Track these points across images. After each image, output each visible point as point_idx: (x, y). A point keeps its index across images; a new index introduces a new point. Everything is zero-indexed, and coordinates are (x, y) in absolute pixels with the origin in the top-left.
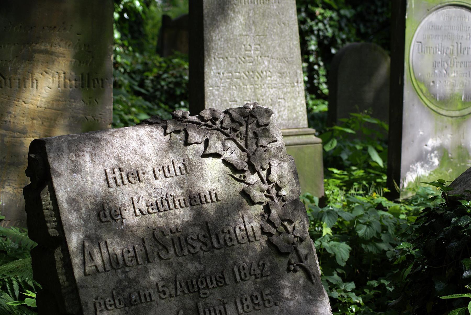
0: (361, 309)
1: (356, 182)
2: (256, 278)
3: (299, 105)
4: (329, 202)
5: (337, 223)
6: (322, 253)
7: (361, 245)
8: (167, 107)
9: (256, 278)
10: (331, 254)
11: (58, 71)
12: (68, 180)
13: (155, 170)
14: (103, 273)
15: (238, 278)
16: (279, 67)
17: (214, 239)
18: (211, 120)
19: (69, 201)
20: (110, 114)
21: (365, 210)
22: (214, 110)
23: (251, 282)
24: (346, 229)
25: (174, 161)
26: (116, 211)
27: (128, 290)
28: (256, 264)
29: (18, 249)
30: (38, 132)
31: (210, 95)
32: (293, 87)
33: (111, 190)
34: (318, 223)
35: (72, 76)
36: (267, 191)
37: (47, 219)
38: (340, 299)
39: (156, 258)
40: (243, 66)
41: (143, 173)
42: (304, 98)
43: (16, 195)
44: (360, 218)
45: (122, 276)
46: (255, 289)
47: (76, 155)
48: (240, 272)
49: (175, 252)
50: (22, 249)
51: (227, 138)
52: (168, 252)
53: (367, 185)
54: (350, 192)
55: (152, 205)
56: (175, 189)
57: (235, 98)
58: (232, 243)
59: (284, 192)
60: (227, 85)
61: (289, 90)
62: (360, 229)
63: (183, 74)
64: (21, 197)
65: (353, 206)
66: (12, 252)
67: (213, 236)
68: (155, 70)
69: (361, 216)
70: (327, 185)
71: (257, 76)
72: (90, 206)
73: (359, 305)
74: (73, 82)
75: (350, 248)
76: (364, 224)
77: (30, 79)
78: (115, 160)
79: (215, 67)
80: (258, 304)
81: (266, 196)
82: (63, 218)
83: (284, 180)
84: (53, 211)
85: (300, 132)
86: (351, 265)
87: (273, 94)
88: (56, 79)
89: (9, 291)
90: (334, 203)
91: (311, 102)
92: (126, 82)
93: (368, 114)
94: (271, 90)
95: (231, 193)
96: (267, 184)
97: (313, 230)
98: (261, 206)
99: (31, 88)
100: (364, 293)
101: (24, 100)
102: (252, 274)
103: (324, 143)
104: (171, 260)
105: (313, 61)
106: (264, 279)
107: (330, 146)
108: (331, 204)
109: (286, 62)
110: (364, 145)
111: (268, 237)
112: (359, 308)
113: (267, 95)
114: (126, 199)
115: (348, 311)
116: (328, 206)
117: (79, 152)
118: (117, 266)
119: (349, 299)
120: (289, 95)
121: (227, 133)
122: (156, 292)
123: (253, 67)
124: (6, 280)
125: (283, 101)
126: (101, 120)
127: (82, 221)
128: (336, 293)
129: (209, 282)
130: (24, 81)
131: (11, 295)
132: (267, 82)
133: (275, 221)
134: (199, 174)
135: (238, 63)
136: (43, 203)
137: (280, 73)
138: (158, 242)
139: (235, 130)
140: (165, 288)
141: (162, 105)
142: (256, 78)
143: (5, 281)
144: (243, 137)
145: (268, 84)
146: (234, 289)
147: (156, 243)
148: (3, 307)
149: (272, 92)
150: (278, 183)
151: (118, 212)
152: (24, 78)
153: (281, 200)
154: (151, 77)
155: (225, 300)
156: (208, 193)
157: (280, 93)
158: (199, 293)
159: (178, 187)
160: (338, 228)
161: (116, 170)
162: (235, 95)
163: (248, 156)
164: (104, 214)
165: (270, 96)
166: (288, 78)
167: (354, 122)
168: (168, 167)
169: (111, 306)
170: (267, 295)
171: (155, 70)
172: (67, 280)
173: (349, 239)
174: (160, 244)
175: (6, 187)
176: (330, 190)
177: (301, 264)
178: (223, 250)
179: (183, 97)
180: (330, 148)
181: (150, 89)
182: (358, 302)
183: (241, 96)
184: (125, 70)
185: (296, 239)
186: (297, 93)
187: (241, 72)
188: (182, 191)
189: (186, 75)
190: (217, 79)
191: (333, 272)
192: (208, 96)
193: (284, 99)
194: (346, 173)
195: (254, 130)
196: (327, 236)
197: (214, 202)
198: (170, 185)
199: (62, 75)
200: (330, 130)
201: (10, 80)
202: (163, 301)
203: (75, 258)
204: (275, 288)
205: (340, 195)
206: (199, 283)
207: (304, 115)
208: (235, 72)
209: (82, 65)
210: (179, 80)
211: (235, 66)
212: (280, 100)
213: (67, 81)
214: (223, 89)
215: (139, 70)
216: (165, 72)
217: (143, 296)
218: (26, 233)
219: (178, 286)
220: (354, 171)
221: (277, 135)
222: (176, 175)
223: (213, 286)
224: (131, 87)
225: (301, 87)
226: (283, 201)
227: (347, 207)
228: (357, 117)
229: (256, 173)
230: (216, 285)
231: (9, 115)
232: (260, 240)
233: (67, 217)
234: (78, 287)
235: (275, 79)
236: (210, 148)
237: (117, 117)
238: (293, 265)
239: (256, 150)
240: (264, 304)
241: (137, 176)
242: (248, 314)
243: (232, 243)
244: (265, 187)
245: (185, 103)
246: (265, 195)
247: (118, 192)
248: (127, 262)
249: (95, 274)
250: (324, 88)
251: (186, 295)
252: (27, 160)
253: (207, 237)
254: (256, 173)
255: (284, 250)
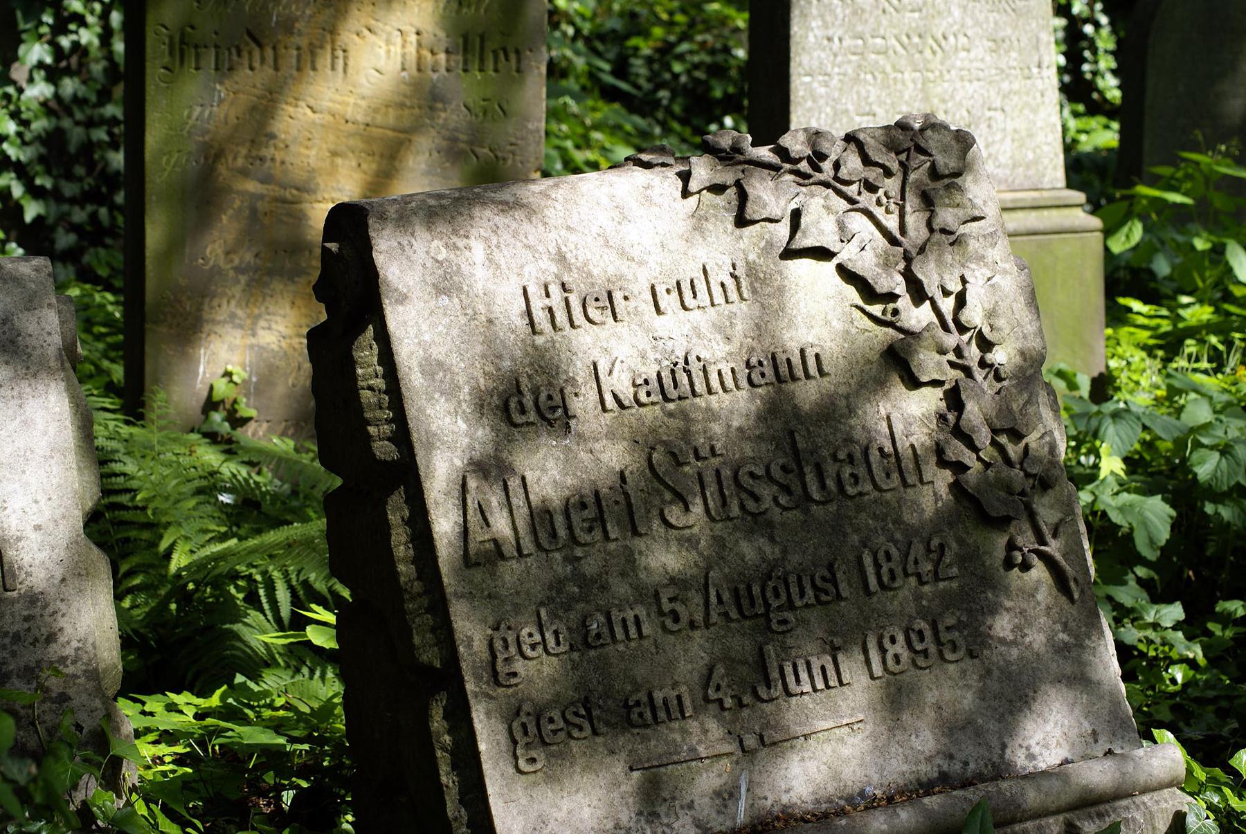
0: (1198, 676)
1: (1192, 337)
2: (921, 583)
3: (1042, 128)
4: (1118, 389)
5: (1137, 446)
6: (1097, 523)
7: (1203, 506)
8: (687, 132)
9: (921, 583)
10: (1120, 527)
11: (402, 28)
12: (426, 314)
13: (657, 289)
14: (514, 562)
15: (872, 581)
16: (992, 25)
17: (810, 478)
18: (809, 159)
19: (427, 369)
20: (538, 143)
21: (1215, 412)
22: (817, 133)
23: (907, 593)
24: (1162, 461)
25: (708, 268)
26: (550, 397)
27: (580, 606)
28: (921, 546)
29: (289, 497)
30: (347, 188)
31: (803, 97)
32: (1029, 78)
33: (539, 340)
34: (1088, 445)
35: (439, 40)
36: (954, 350)
37: (368, 415)
38: (1142, 647)
39: (656, 523)
40: (895, 21)
41: (626, 298)
42: (1058, 107)
43: (285, 353)
44: (1203, 432)
45: (563, 570)
46: (918, 613)
47: (447, 246)
48: (878, 566)
49: (707, 510)
50: (301, 496)
51: (850, 207)
52: (687, 509)
53: (1221, 347)
54: (1174, 365)
55: (646, 382)
56: (710, 341)
57: (870, 105)
58: (859, 488)
59: (999, 356)
60: (850, 71)
61: (1016, 86)
62: (1202, 462)
63: (731, 43)
64: (300, 359)
65: (1182, 402)
66: (273, 503)
67: (807, 469)
68: (658, 32)
69: (1206, 427)
70: (1112, 342)
71: (931, 48)
72: (482, 381)
73: (1192, 664)
74: (442, 57)
75: (1174, 513)
76: (1212, 448)
77: (329, 47)
78: (552, 260)
79: (820, 23)
80: (925, 653)
81: (952, 365)
82: (411, 412)
83: (1001, 322)
84: (385, 393)
85: (1044, 199)
86: (1175, 559)
87: (972, 97)
88: (397, 49)
89: (266, 606)
90: (1131, 392)
91: (1073, 124)
92: (580, 63)
93: (1227, 154)
94: (967, 84)
95: (859, 356)
96: (956, 333)
97: (1074, 463)
98: (939, 392)
99: (329, 72)
100: (1210, 634)
101: (312, 102)
102: (910, 571)
103: (1108, 232)
104: (696, 530)
105: (1081, 12)
106: (941, 585)
107: (1123, 238)
108: (1123, 395)
109: (1009, 10)
110: (1214, 239)
111: (954, 474)
112: (1191, 673)
113: (958, 98)
114: (579, 364)
115: (1162, 680)
116: (1115, 398)
117: (455, 239)
118: (550, 543)
119: (1167, 649)
120: (1016, 98)
121: (850, 194)
122: (653, 615)
123: (921, 23)
124: (259, 578)
125: (998, 115)
126: (514, 160)
127: (460, 422)
128: (1134, 631)
129: (794, 590)
130: (313, 54)
131: (270, 617)
132: (958, 63)
133: (974, 432)
134: (774, 302)
135: (880, 12)
136: (360, 371)
137: (994, 41)
138: (661, 480)
139: (871, 188)
140: (678, 603)
141: (676, 126)
142: (928, 53)
143: (255, 581)
144: (893, 207)
145: (961, 70)
146: (862, 612)
147: (656, 484)
148: (250, 648)
149: (971, 92)
150: (986, 331)
151: (558, 398)
152: (311, 44)
153: (991, 376)
154: (646, 50)
155: (837, 641)
156: (797, 353)
157: (992, 93)
158: (769, 620)
159: (718, 337)
160: (1142, 458)
161: (555, 290)
162: (872, 99)
163: (908, 258)
164: (520, 403)
165: (964, 102)
166: (1014, 54)
167: (1188, 177)
168: (692, 281)
169: (533, 647)
170: (948, 629)
171: (658, 32)
172: (419, 578)
173: (1170, 487)
174: (668, 487)
175: (261, 332)
176: (1121, 357)
177: (1043, 548)
178: (835, 508)
179: (730, 105)
180: (1124, 243)
181: (642, 82)
182: (1191, 656)
183: (889, 101)
184: (578, 31)
185: (1031, 481)
186: (1038, 95)
187: (887, 36)
188: (727, 348)
189: (739, 44)
190: (823, 55)
191: (1127, 574)
192: (800, 100)
193: (1003, 110)
194: (1164, 312)
195: (923, 188)
196: (1111, 479)
197: (814, 378)
198: (696, 330)
199: (413, 38)
200: (1124, 198)
201: (274, 48)
202: (672, 638)
203: (441, 520)
204: (970, 611)
205: (1148, 371)
206: (769, 594)
207: (1056, 155)
208: (873, 37)
209: (465, 10)
210: (720, 58)
211: (872, 20)
212: (992, 113)
213: (426, 54)
214: (840, 81)
215: (614, 31)
216: (684, 37)
217: (620, 625)
218: (311, 455)
219: (713, 599)
220: (1188, 306)
221: (985, 202)
222: (713, 305)
223: (805, 601)
224: (593, 75)
225: (1049, 82)
226: (998, 378)
227: (1167, 404)
228: (1197, 163)
229: (928, 302)
230: (812, 601)
231: (272, 142)
232: (932, 482)
233: (421, 410)
234: (448, 596)
235: (980, 56)
236: (804, 233)
237: (555, 153)
238: (1020, 549)
239: (928, 240)
240: (941, 653)
241: (608, 304)
242: (898, 677)
243: (859, 488)
244: (951, 340)
245: (734, 120)
246: (949, 362)
247: (557, 345)
248: (578, 532)
249: (494, 564)
250: (1110, 87)
251: (733, 625)
252: (317, 263)
253: (792, 471)
254: (928, 302)
255: (997, 510)
